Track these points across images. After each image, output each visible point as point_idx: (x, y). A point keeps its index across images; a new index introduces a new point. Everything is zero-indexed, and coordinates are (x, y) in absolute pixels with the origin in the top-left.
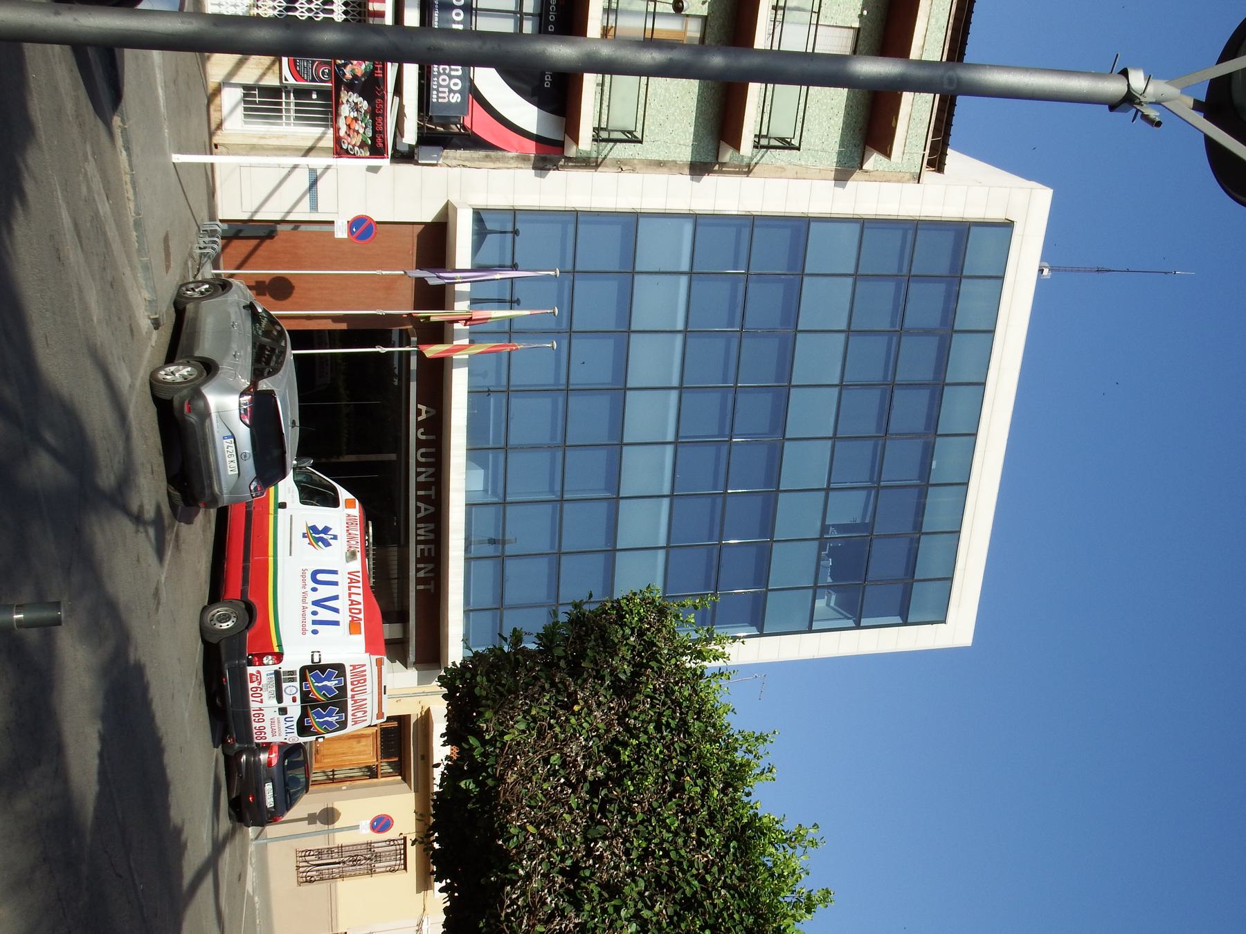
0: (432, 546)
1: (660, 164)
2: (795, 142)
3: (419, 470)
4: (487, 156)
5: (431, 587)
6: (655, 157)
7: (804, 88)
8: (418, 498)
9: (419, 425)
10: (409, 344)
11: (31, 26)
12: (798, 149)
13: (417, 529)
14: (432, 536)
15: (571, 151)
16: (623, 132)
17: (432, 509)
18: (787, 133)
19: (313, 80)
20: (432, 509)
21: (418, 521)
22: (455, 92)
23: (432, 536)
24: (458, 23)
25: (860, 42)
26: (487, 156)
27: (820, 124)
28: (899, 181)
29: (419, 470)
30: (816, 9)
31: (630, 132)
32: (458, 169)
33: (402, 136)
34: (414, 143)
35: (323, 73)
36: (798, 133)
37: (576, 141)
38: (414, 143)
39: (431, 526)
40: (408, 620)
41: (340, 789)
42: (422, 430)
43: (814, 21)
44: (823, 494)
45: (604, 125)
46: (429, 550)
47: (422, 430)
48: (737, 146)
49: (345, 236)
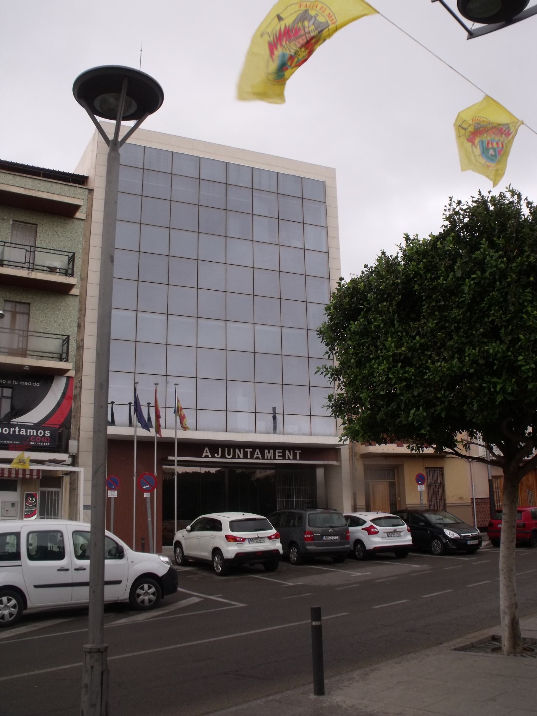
0: (277, 451)
1: (79, 326)
2: (70, 255)
3: (237, 457)
4: (74, 417)
5: (298, 452)
6: (75, 329)
7: (365, 507)
8: (252, 458)
9: (213, 456)
10: (174, 461)
11: (55, 606)
12: (74, 253)
13: (267, 459)
14: (272, 451)
15: (72, 373)
16: (63, 345)
17: (257, 451)
18: (66, 259)
19: (35, 506)
20: (257, 451)
21: (263, 458)
22: (45, 434)
23: (272, 451)
24: (10, 431)
25: (20, 220)
26: (74, 417)
27: (61, 241)
28: (92, 201)
29: (237, 457)
30: (3, 244)
31: (64, 341)
32: (81, 432)
33: (65, 461)
34: (68, 455)
35: (32, 500)
36: (66, 253)
37: (67, 371)
38: (68, 455)
39: (266, 451)
40: (315, 464)
41: (400, 501)
42: (216, 455)
43: (9, 245)
44: (254, 216)
45: (58, 356)
46: (279, 453)
47: (216, 455)
48: (71, 286)
49: (116, 492)
